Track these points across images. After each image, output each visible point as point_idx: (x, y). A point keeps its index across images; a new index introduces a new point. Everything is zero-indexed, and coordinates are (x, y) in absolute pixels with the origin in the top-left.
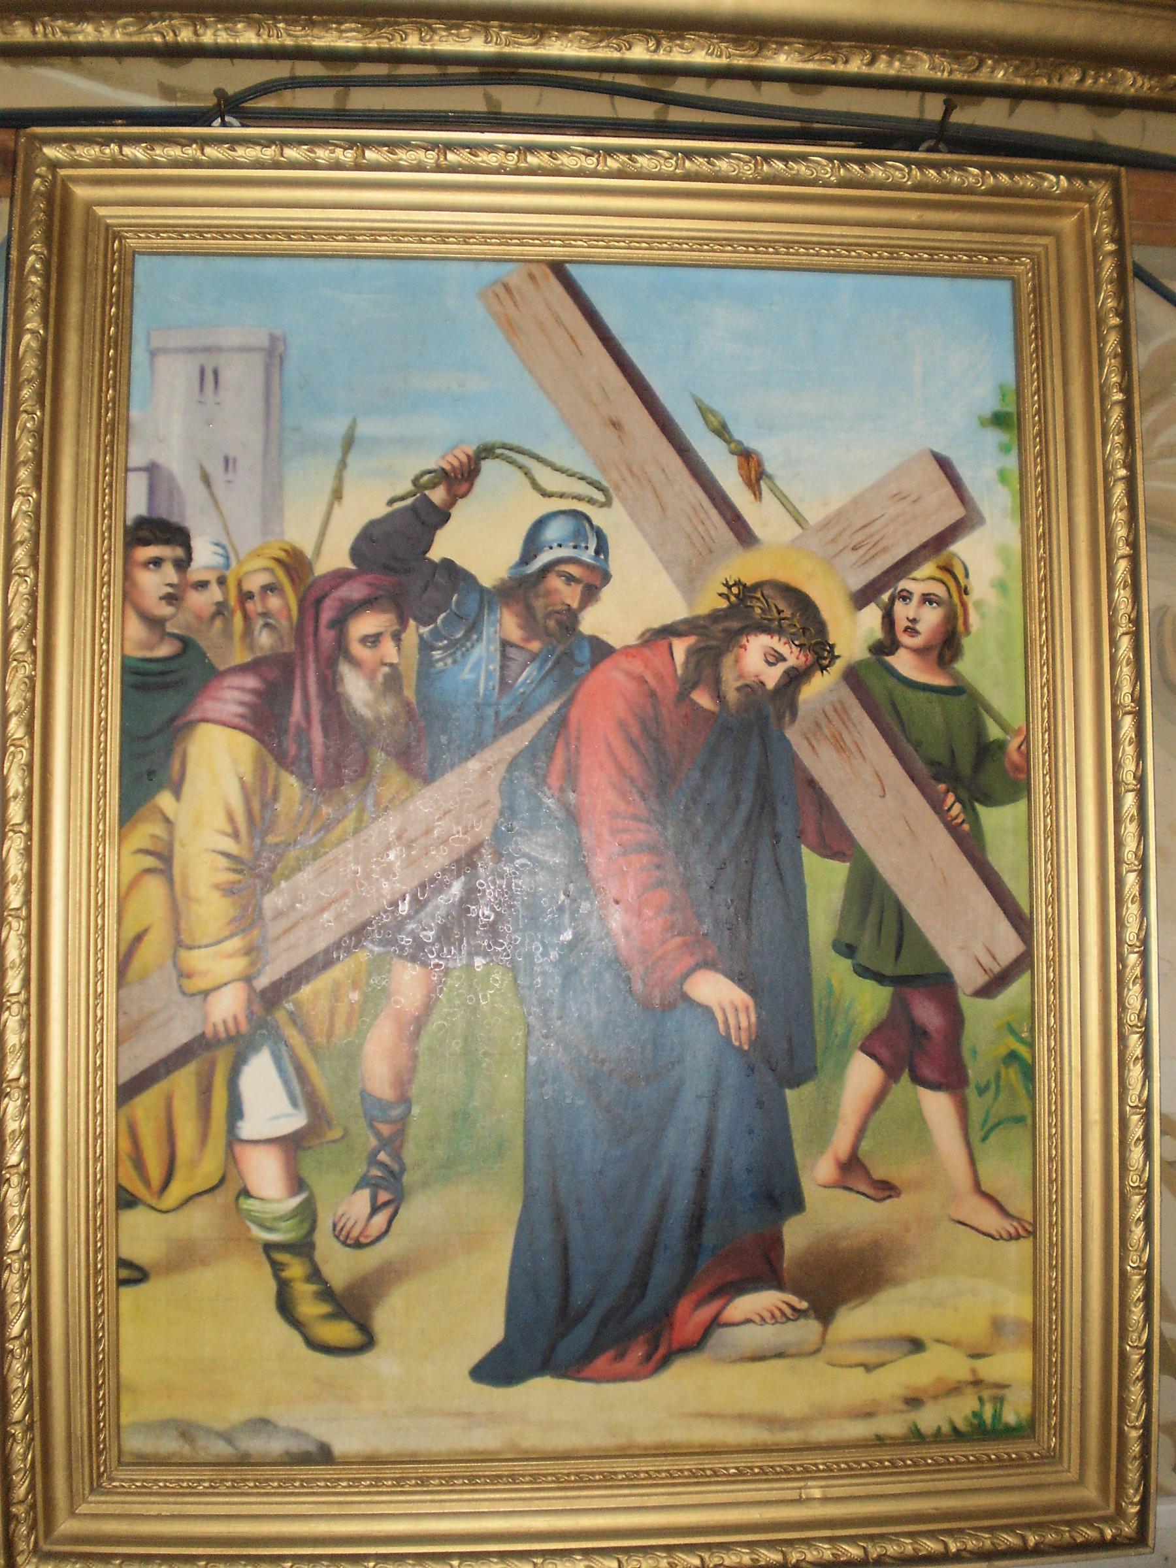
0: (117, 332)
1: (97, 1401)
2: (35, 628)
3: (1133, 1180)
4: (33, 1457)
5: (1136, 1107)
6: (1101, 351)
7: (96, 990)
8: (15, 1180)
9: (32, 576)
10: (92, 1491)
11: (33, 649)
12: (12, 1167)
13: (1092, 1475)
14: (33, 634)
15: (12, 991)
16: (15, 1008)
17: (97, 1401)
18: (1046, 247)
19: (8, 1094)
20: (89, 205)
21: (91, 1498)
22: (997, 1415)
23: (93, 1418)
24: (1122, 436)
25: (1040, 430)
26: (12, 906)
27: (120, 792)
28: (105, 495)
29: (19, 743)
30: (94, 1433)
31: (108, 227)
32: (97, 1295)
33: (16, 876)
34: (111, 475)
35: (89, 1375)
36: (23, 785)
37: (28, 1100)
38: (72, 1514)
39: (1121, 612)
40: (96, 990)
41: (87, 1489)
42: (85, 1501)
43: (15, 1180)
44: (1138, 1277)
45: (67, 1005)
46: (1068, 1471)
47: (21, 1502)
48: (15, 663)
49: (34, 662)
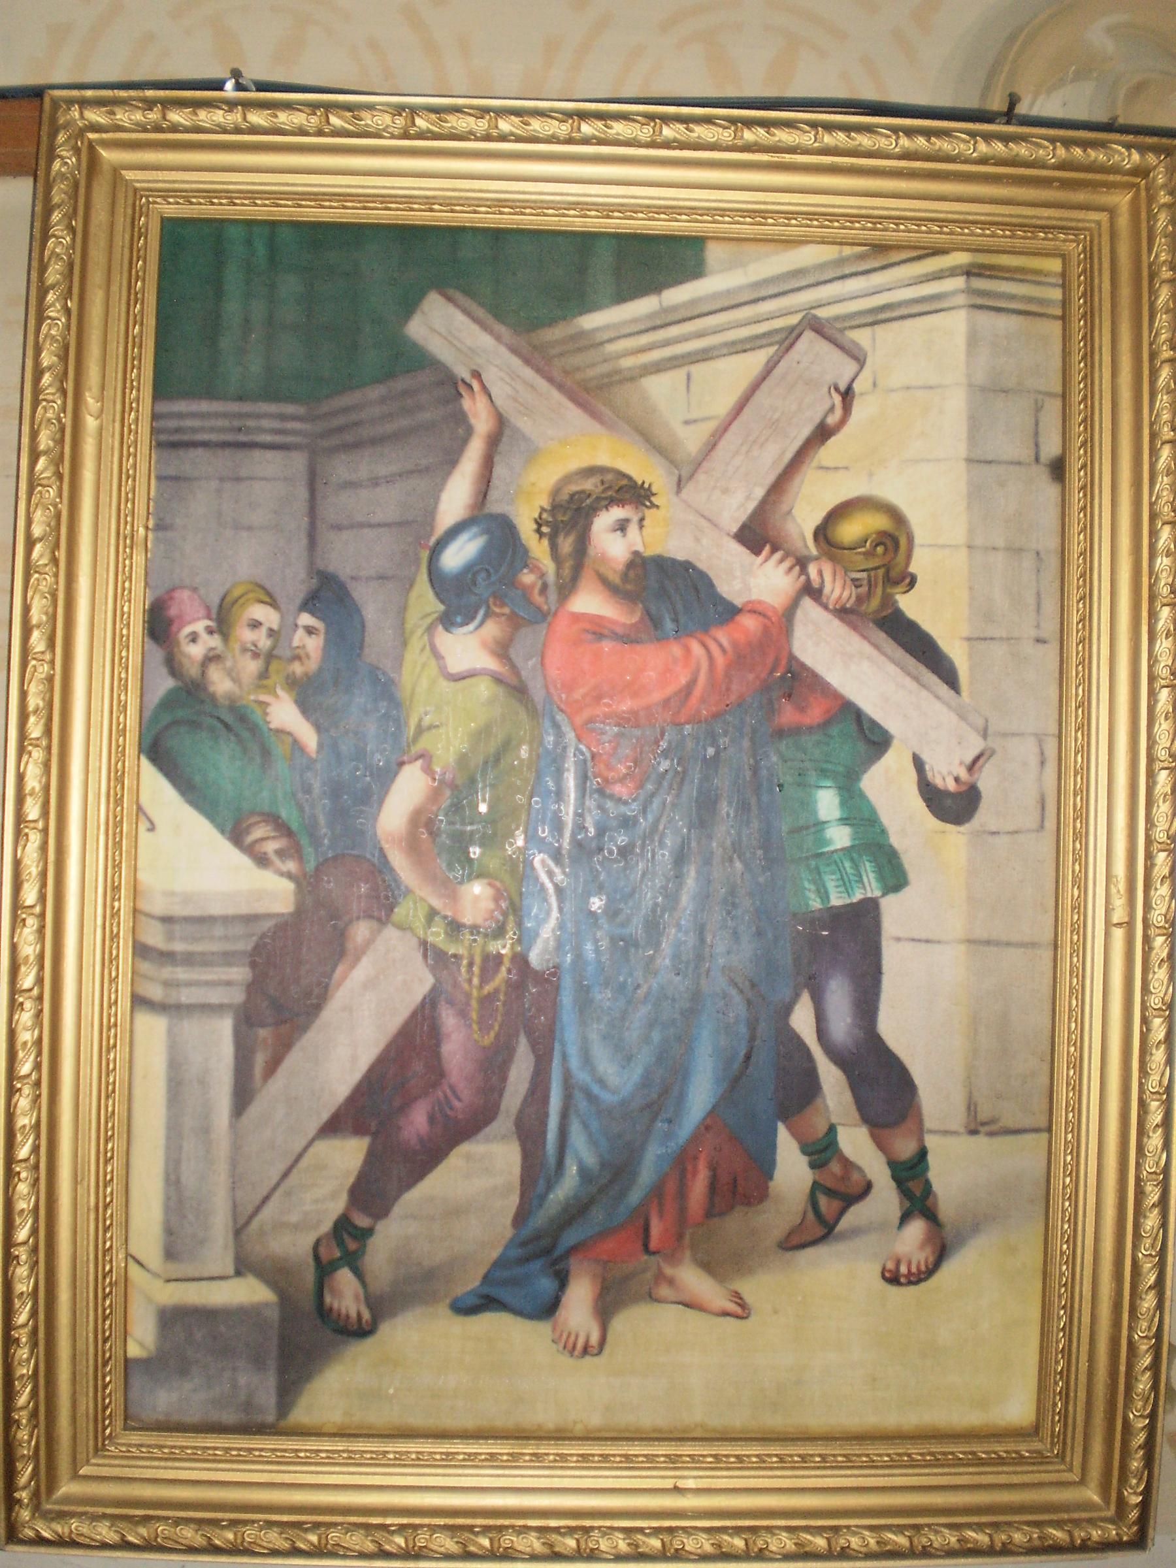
0: (141, 331)
1: (104, 1310)
2: (66, 373)
3: (1149, 1167)
4: (37, 1443)
5: (1160, 1009)
6: (1152, 305)
7: (112, 931)
8: (28, 1005)
9: (59, 402)
10: (96, 1450)
11: (60, 477)
12: (21, 1161)
13: (1095, 1472)
14: (57, 546)
15: (30, 818)
16: (27, 1090)
17: (104, 1310)
18: (1099, 223)
19: (20, 1090)
20: (116, 171)
21: (93, 1461)
22: (1055, 275)
23: (100, 1327)
24: (1116, 1538)
25: (1086, 417)
26: (33, 736)
27: (157, 319)
28: (126, 523)
29: (51, 397)
30: (100, 1277)
31: (136, 190)
32: (106, 1162)
33: (33, 788)
34: (139, 368)
35: (97, 1238)
36: (40, 782)
37: (40, 1095)
38: (75, 1477)
39: (1163, 583)
40: (112, 931)
41: (91, 1450)
42: (88, 1462)
43: (27, 1090)
44: (1157, 1103)
45: (79, 1033)
46: (1071, 1470)
47: (22, 1408)
48: (36, 576)
49: (56, 575)
